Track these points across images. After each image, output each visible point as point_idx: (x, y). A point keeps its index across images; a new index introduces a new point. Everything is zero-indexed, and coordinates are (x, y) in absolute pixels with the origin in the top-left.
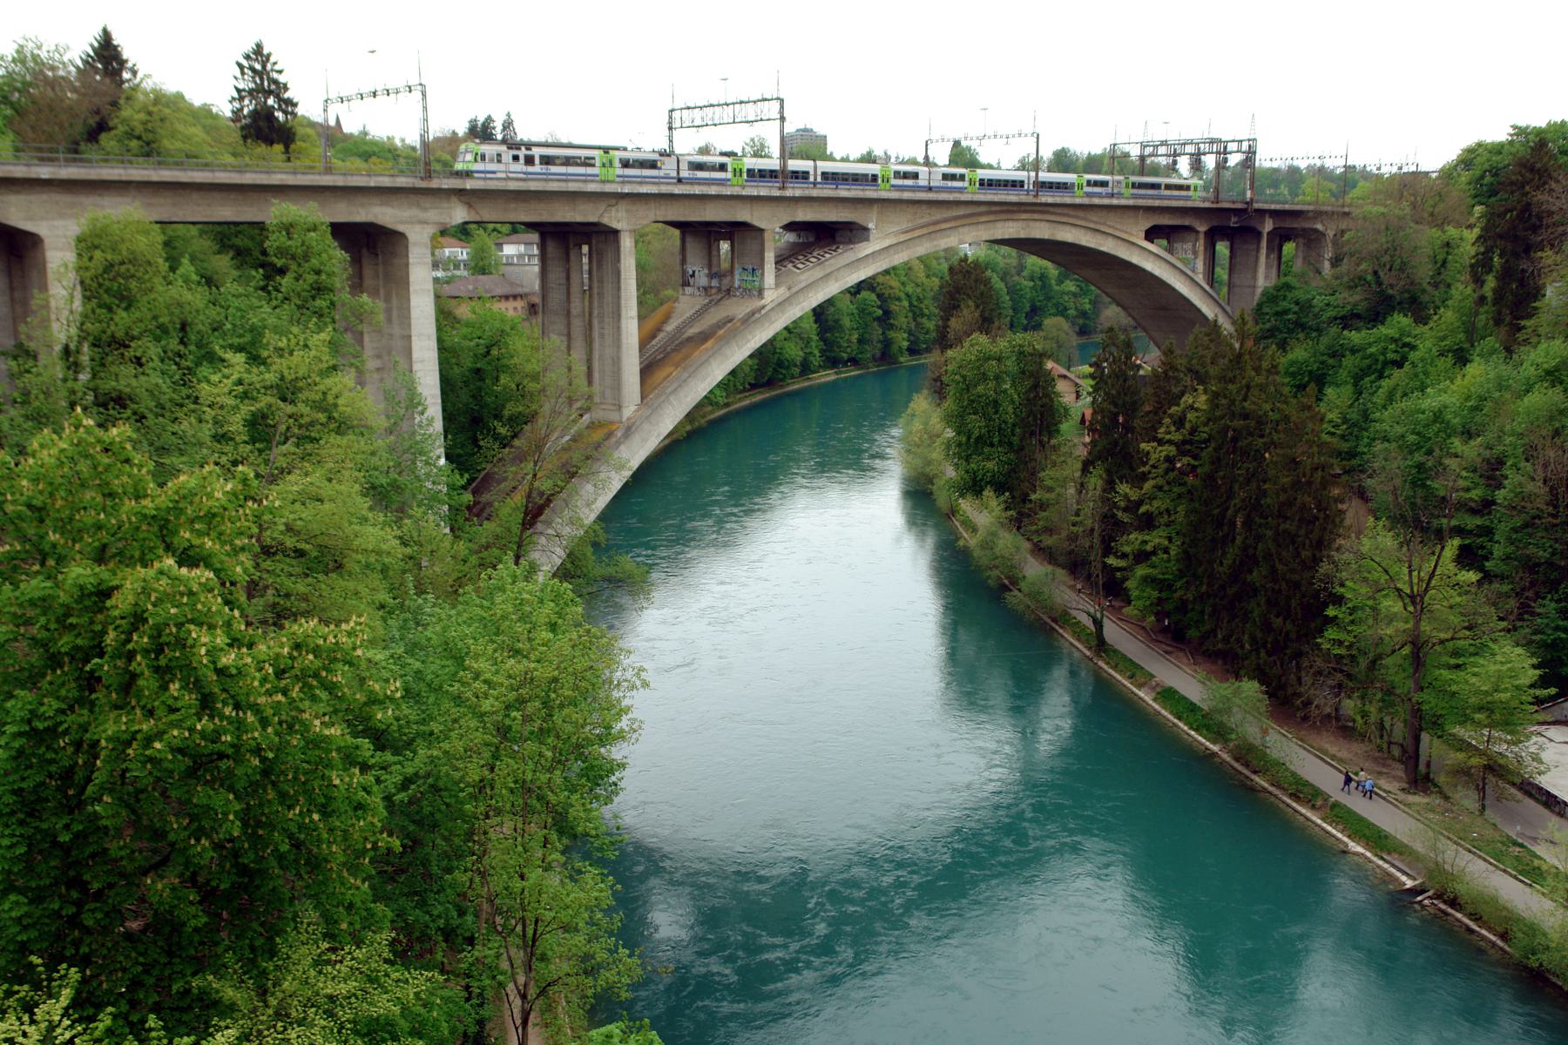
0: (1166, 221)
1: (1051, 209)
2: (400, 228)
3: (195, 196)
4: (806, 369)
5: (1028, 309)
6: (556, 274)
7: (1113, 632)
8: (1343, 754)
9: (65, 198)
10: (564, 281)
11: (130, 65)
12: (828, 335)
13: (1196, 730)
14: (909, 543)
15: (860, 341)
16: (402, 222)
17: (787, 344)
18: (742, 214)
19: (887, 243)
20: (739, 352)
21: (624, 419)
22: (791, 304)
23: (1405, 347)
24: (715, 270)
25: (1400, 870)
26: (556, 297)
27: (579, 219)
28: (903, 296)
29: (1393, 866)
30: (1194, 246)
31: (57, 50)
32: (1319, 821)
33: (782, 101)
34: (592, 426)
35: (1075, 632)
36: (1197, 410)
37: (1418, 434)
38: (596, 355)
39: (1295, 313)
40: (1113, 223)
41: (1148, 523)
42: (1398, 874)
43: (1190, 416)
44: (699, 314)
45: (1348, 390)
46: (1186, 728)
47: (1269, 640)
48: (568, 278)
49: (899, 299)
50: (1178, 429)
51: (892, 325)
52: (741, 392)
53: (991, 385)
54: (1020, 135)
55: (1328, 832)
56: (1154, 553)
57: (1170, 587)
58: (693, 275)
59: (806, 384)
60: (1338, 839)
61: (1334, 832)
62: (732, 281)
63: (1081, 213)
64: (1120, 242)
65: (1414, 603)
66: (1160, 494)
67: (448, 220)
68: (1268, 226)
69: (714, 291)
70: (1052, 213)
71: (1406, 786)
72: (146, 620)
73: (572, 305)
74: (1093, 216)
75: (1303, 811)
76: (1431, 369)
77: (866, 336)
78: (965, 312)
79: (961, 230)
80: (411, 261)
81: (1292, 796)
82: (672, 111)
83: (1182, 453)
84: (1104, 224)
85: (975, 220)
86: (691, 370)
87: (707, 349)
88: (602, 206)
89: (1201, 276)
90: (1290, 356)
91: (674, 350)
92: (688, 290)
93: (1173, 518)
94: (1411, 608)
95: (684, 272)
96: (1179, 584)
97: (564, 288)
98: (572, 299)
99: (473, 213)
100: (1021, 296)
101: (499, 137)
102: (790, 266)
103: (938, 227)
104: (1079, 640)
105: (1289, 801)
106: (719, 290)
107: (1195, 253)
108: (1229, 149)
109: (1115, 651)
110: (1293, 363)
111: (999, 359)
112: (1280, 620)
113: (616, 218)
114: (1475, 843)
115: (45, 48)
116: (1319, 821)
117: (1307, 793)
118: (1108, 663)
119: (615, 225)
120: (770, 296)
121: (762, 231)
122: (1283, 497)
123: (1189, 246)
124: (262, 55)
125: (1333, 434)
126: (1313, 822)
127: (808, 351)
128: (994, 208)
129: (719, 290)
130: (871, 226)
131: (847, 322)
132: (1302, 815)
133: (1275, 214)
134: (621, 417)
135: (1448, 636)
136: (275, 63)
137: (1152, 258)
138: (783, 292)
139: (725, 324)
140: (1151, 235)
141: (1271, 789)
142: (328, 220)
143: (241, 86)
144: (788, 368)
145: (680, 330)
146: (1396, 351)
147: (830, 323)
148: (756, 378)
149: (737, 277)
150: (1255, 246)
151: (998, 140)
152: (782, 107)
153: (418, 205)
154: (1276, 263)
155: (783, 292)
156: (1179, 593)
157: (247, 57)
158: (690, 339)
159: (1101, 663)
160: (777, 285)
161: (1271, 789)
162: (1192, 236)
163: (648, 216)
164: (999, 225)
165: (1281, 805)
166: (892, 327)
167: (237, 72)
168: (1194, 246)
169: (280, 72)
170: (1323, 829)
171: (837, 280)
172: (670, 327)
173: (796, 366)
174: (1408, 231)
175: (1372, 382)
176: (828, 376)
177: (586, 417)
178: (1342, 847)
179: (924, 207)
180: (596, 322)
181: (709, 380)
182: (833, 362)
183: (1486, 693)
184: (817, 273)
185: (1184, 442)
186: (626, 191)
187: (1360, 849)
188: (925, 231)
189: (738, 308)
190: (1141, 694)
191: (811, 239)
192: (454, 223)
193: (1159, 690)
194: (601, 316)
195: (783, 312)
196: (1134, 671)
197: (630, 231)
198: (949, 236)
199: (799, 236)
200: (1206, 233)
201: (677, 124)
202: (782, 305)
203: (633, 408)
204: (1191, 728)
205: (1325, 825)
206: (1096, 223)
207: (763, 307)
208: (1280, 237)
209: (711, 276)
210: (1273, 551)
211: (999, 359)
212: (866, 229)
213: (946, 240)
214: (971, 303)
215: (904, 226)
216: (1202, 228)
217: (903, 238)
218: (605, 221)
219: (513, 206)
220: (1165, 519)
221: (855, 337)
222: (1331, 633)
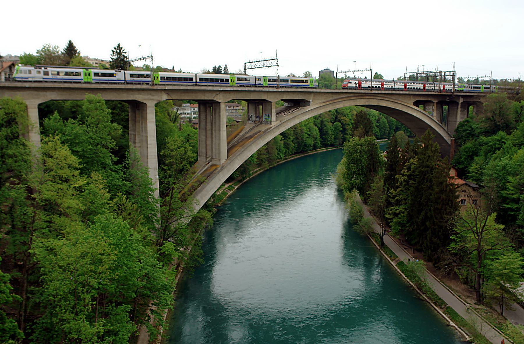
0: (421, 99)
1: (378, 95)
2: (144, 102)
3: (77, 92)
4: (315, 147)
5: (395, 128)
6: (203, 117)
7: (387, 239)
8: (458, 289)
9: (35, 93)
10: (205, 119)
11: (78, 51)
12: (324, 136)
13: (407, 277)
14: (336, 207)
15: (335, 138)
16: (145, 100)
17: (307, 139)
18: (264, 97)
19: (316, 106)
20: (261, 143)
21: (221, 164)
22: (281, 127)
23: (502, 142)
24: (257, 115)
25: (466, 333)
26: (203, 124)
27: (206, 99)
28: (350, 123)
29: (464, 332)
30: (433, 107)
31: (55, 48)
32: (442, 313)
33: (277, 60)
34: (212, 165)
35: (376, 240)
36: (414, 164)
37: (497, 174)
38: (214, 143)
39: (470, 131)
40: (401, 99)
41: (398, 203)
42: (465, 335)
43: (413, 166)
44: (251, 129)
45: (483, 157)
46: (404, 276)
47: (432, 246)
48: (206, 118)
49: (349, 125)
50: (408, 171)
51: (346, 133)
52: (291, 155)
53: (358, 154)
54: (366, 70)
55: (444, 317)
56: (399, 214)
57: (405, 226)
58: (251, 117)
59: (315, 152)
60: (447, 320)
61: (446, 317)
62: (263, 119)
63: (388, 96)
64: (404, 106)
65: (478, 236)
66: (403, 193)
67: (160, 99)
68: (461, 100)
69: (257, 122)
70: (372, 96)
71: (476, 302)
72: (92, 224)
73: (207, 126)
74: (393, 97)
75: (437, 309)
76: (510, 151)
77: (337, 137)
78: (359, 129)
79: (344, 102)
80: (148, 112)
81: (434, 303)
82: (246, 63)
83: (411, 179)
84: (398, 100)
85: (349, 99)
86: (245, 148)
87: (251, 141)
88: (214, 94)
89: (435, 118)
90: (466, 146)
91: (241, 141)
92: (249, 121)
93: (407, 201)
94: (477, 237)
95: (248, 116)
96: (407, 225)
97: (205, 121)
98: (207, 125)
99: (169, 96)
100: (392, 124)
101: (223, 72)
102: (283, 114)
103: (335, 101)
104: (377, 243)
105: (433, 305)
106: (259, 122)
107: (433, 110)
108: (446, 75)
109: (387, 247)
110: (467, 148)
111: (361, 145)
112: (436, 239)
113: (219, 98)
114: (496, 325)
115: (51, 47)
116: (442, 313)
117: (440, 303)
118: (384, 252)
119: (219, 101)
120: (274, 124)
121: (219, 103)
122: (436, 196)
123: (431, 107)
124: (120, 48)
125: (476, 173)
126: (440, 313)
127: (316, 141)
128: (356, 95)
129: (259, 122)
130: (310, 101)
131: (330, 132)
132: (437, 310)
133: (463, 96)
134: (220, 163)
135: (490, 247)
136: (124, 50)
137: (416, 112)
138: (278, 122)
139: (258, 133)
140: (417, 104)
141: (428, 300)
142: (104, 99)
143: (113, 57)
144: (308, 147)
145: (244, 135)
146: (499, 145)
147: (324, 132)
148: (297, 150)
149: (264, 118)
150: (456, 108)
151: (359, 72)
152: (277, 61)
153: (150, 94)
154: (466, 113)
155: (278, 122)
156: (408, 228)
157: (115, 48)
158: (246, 138)
159: (382, 252)
160: (276, 120)
161: (428, 300)
162: (432, 104)
163: (280, 97)
164: (358, 100)
165: (430, 306)
166: (346, 134)
167: (112, 53)
168: (433, 107)
169: (125, 53)
170: (443, 316)
171: (298, 119)
172: (241, 134)
173: (311, 146)
174: (506, 102)
175: (491, 155)
176: (324, 150)
177: (210, 163)
178: (448, 323)
179: (330, 94)
180: (214, 132)
181: (252, 151)
182: (325, 145)
183: (500, 270)
184: (291, 116)
185: (410, 175)
186: (222, 89)
187: (454, 325)
188: (330, 102)
189: (263, 128)
190: (392, 263)
191: (293, 105)
192: (163, 100)
193: (398, 262)
194: (215, 130)
195: (279, 129)
196: (392, 255)
197: (224, 103)
198: (339, 104)
199: (289, 104)
200: (437, 103)
201: (247, 68)
202: (278, 127)
203: (225, 160)
204: (406, 276)
205: (443, 315)
206: (394, 99)
207: (271, 127)
208: (466, 105)
209: (256, 117)
210: (433, 215)
211: (361, 145)
212: (309, 102)
213: (338, 106)
214: (362, 126)
215: (323, 101)
216: (435, 101)
217: (322, 105)
218: (215, 99)
219: (183, 94)
220: (404, 202)
221: (333, 137)
222: (453, 245)
